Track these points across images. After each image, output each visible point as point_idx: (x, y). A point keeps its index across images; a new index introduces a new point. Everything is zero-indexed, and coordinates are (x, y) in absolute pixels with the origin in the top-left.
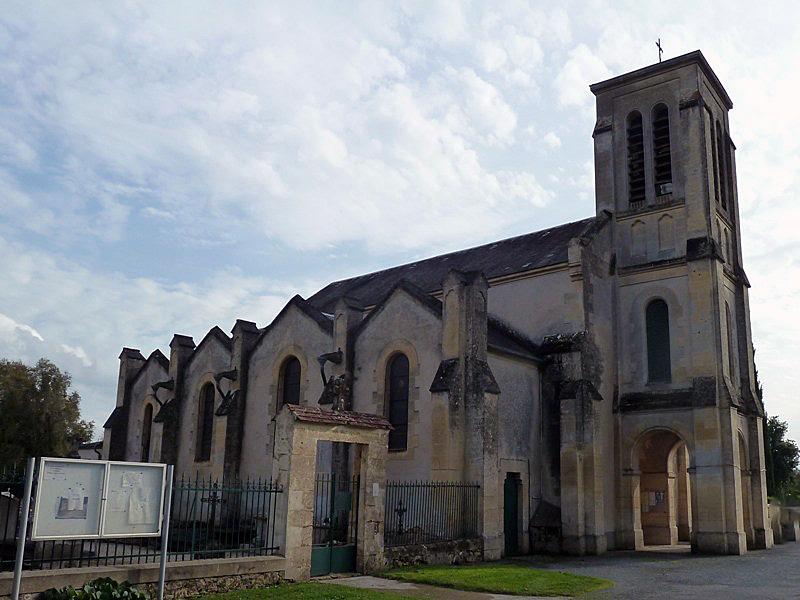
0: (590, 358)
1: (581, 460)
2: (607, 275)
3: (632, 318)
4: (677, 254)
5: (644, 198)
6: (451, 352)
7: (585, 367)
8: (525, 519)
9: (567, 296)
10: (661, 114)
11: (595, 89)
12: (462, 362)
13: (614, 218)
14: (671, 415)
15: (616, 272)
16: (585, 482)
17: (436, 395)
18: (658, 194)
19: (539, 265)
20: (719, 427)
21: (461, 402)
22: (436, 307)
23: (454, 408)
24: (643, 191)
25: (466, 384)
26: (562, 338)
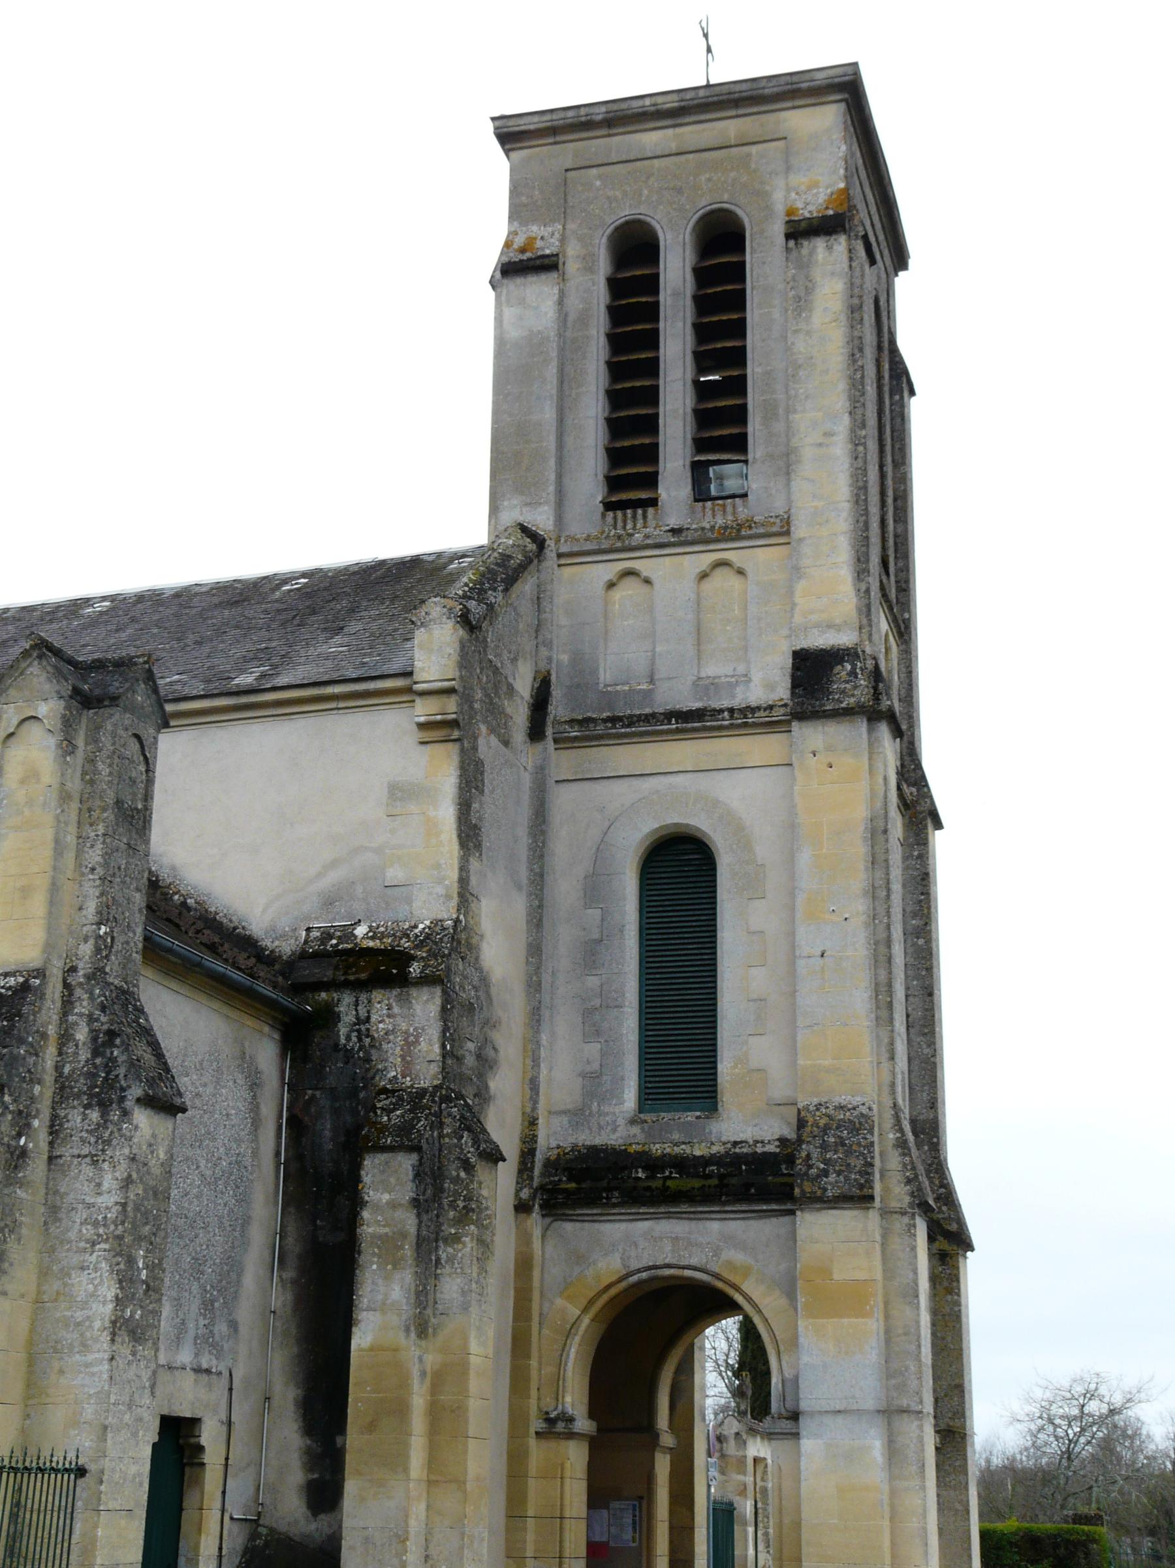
1: (423, 1374)
3: (595, 889)
4: (755, 694)
5: (654, 502)
7: (449, 1035)
9: (399, 793)
10: (721, 239)
11: (512, 134)
12: (54, 990)
13: (550, 553)
14: (715, 1226)
15: (549, 731)
16: (433, 1461)
18: (701, 494)
20: (879, 1276)
24: (651, 481)
25: (58, 1068)
26: (374, 934)
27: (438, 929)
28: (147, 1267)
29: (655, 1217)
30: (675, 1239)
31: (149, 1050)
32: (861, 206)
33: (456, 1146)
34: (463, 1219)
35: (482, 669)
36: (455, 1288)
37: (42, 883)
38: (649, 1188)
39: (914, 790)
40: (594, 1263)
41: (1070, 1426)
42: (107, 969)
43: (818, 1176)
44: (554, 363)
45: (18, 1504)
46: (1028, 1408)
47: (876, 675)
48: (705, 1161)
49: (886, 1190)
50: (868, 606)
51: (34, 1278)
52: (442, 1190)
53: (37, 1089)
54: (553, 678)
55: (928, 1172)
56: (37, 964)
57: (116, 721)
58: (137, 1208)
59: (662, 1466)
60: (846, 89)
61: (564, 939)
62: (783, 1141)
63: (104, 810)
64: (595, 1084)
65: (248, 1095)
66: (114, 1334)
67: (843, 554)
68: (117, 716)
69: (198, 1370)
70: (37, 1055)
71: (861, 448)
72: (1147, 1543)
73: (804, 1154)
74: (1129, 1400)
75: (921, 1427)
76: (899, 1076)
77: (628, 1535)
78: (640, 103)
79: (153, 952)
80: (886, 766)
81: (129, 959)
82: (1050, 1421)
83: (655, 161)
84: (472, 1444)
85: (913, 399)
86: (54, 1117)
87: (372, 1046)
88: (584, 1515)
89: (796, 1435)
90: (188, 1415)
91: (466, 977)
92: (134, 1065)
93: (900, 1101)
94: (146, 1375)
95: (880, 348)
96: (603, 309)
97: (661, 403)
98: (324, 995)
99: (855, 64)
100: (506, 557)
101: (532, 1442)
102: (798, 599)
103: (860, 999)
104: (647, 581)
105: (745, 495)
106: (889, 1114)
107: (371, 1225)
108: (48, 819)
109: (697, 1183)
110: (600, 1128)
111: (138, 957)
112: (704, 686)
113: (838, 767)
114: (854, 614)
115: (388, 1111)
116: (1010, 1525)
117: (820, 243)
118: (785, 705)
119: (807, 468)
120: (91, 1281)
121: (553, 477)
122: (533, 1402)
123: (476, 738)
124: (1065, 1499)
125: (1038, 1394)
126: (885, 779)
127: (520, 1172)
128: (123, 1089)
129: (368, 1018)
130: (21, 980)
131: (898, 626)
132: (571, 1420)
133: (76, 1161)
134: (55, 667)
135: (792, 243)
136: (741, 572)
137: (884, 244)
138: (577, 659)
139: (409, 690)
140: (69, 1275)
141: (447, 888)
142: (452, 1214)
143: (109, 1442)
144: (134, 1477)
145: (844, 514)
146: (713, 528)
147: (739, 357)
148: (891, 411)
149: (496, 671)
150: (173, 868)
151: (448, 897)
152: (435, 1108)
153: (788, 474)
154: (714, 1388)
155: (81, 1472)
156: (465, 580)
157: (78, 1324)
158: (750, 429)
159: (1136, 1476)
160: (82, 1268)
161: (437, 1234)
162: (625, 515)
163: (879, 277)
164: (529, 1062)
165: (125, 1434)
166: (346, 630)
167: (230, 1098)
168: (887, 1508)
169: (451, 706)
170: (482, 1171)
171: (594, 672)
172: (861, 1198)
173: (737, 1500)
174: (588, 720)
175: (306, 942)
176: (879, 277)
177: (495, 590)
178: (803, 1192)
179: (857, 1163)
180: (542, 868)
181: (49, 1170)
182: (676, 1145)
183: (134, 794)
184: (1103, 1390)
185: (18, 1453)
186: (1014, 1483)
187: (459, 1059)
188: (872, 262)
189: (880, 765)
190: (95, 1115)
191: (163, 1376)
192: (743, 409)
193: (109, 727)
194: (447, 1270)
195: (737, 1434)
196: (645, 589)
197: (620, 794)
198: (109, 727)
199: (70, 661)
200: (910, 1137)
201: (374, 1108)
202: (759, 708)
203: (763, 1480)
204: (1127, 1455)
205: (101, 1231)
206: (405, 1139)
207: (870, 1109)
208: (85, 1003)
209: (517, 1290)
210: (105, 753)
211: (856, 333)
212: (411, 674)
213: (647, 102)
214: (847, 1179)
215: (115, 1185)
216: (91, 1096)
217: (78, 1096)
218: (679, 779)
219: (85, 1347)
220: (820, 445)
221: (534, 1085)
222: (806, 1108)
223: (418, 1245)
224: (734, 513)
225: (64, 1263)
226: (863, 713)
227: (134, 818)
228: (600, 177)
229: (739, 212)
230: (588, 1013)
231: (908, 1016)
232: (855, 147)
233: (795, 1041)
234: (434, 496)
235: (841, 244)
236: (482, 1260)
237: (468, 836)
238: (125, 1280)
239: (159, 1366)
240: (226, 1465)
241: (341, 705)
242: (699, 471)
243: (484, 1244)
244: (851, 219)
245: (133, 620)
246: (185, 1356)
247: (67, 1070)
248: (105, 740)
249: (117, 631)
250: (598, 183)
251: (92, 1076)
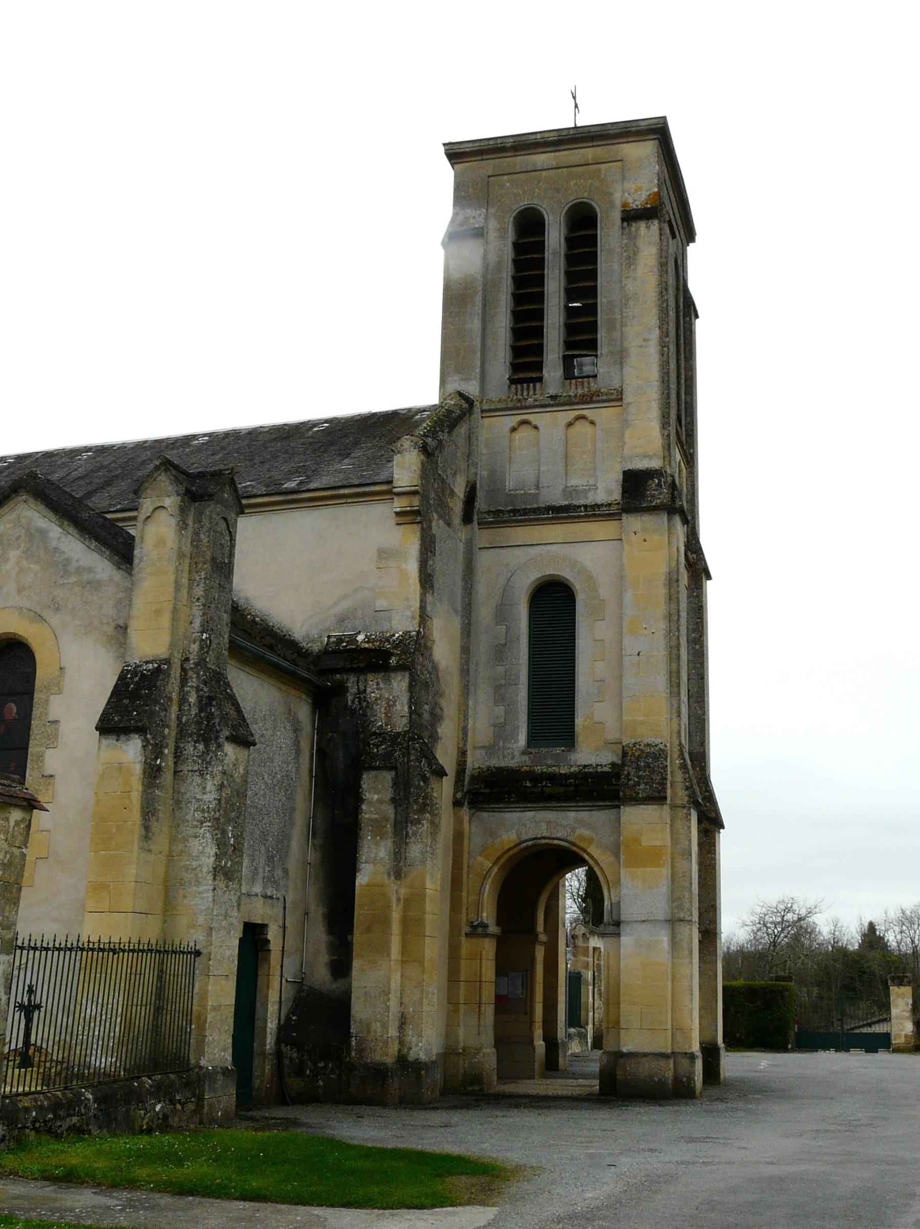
0: (423, 687)
1: (399, 900)
2: (457, 520)
3: (502, 613)
4: (600, 497)
5: (540, 379)
6: (150, 643)
7: (414, 701)
8: (272, 1025)
9: (384, 554)
10: (583, 221)
11: (456, 154)
12: (176, 672)
14: (572, 815)
17: (110, 741)
18: (569, 374)
19: (313, 486)
20: (669, 843)
21: (167, 762)
22: (122, 551)
23: (152, 773)
24: (539, 366)
25: (179, 718)
26: (368, 640)
27: (407, 637)
28: (233, 836)
29: (536, 809)
31: (233, 708)
32: (667, 202)
33: (418, 767)
34: (423, 809)
35: (435, 479)
36: (418, 850)
37: (168, 607)
38: (533, 793)
39: (695, 556)
40: (501, 836)
41: (775, 927)
42: (208, 660)
43: (634, 785)
44: (480, 294)
45: (162, 971)
46: (752, 918)
47: (673, 486)
48: (567, 776)
49: (674, 794)
50: (669, 445)
51: (167, 842)
52: (410, 793)
53: (166, 731)
54: (478, 485)
55: (698, 783)
56: (165, 656)
57: (212, 510)
58: (227, 803)
59: (540, 953)
60: (658, 132)
61: (483, 645)
62: (613, 765)
63: (205, 563)
64: (501, 730)
65: (292, 735)
66: (215, 875)
67: (654, 414)
68: (212, 507)
69: (265, 897)
70: (166, 710)
71: (666, 349)
72: (816, 990)
73: (626, 772)
74: (809, 913)
75: (691, 930)
76: (683, 727)
77: (519, 991)
78: (534, 137)
79: (235, 650)
80: (678, 541)
81: (221, 653)
82: (765, 925)
83: (544, 173)
84: (427, 940)
85: (697, 320)
86: (177, 748)
87: (367, 707)
88: (493, 980)
89: (619, 935)
90: (260, 922)
91: (424, 666)
92: (224, 717)
93: (683, 742)
94: (234, 899)
95: (678, 289)
96: (510, 260)
97: (545, 302)
98: (338, 676)
99: (665, 117)
100: (450, 412)
101: (463, 939)
102: (626, 439)
103: (660, 681)
104: (536, 428)
105: (596, 376)
106: (676, 750)
107: (368, 813)
108: (171, 569)
109: (562, 790)
110: (504, 757)
111: (226, 653)
112: (569, 491)
113: (647, 542)
114: (661, 450)
115: (377, 746)
116: (740, 982)
117: (642, 225)
118: (618, 504)
119: (633, 360)
120: (201, 844)
121: (479, 363)
122: (464, 916)
123: (430, 521)
124: (772, 968)
125: (759, 910)
126: (678, 549)
127: (456, 782)
128: (218, 732)
129: (365, 690)
130: (156, 665)
131: (686, 457)
132: (486, 926)
133: (190, 774)
134: (174, 476)
135: (625, 224)
136: (592, 423)
137: (681, 227)
138: (492, 474)
139: (390, 492)
140: (188, 840)
141: (413, 612)
142: (415, 807)
143: (214, 937)
144: (229, 958)
145: (655, 389)
146: (576, 396)
147: (592, 292)
148: (684, 328)
149: (443, 481)
150: (247, 599)
151: (413, 618)
152: (405, 745)
153: (622, 363)
154: (570, 909)
155: (198, 953)
156: (425, 425)
157: (194, 869)
158: (599, 336)
159: (812, 954)
160: (196, 837)
161: (407, 818)
162: (523, 387)
163: (678, 246)
164: (462, 717)
165: (223, 932)
166: (352, 455)
167: (282, 738)
168: (670, 975)
169: (416, 501)
170: (434, 782)
171: (503, 481)
172: (658, 798)
173: (583, 971)
174: (499, 511)
175: (327, 644)
176: (678, 246)
177: (443, 432)
178: (625, 795)
179: (657, 778)
180: (470, 600)
181: (175, 779)
182: (551, 767)
183: (223, 554)
184: (795, 907)
185: (161, 942)
186: (745, 960)
187: (420, 715)
188: (674, 237)
189: (675, 541)
190: (201, 747)
191: (245, 900)
192: (595, 323)
193: (208, 513)
194: (413, 839)
195: (584, 934)
196: (534, 432)
197: (518, 556)
198: (208, 513)
199: (184, 473)
200: (689, 762)
201: (369, 744)
202: (602, 505)
203: (598, 960)
204: (807, 942)
205: (206, 815)
207: (666, 746)
208: (194, 680)
209: (454, 852)
210: (205, 529)
211: (664, 280)
212: (391, 482)
213: (539, 136)
214: (651, 787)
215: (214, 788)
216: (199, 735)
217: (191, 735)
218: (554, 547)
219: (198, 883)
220: (641, 346)
221: (464, 731)
222: (628, 745)
223: (395, 825)
224: (589, 387)
225: (185, 834)
226: (665, 509)
227: (223, 568)
228: (509, 181)
229: (594, 204)
230: (497, 689)
231: (689, 691)
232: (664, 167)
233: (621, 706)
234: (406, 373)
235: (655, 225)
236: (434, 834)
237: (425, 581)
238: (221, 844)
239: (242, 894)
240: (283, 951)
241: (349, 501)
242: (568, 361)
243: (435, 825)
244: (661, 210)
245: (223, 448)
246: (257, 889)
247: (184, 720)
248: (205, 521)
249: (213, 455)
250: (508, 185)
251: (199, 723)
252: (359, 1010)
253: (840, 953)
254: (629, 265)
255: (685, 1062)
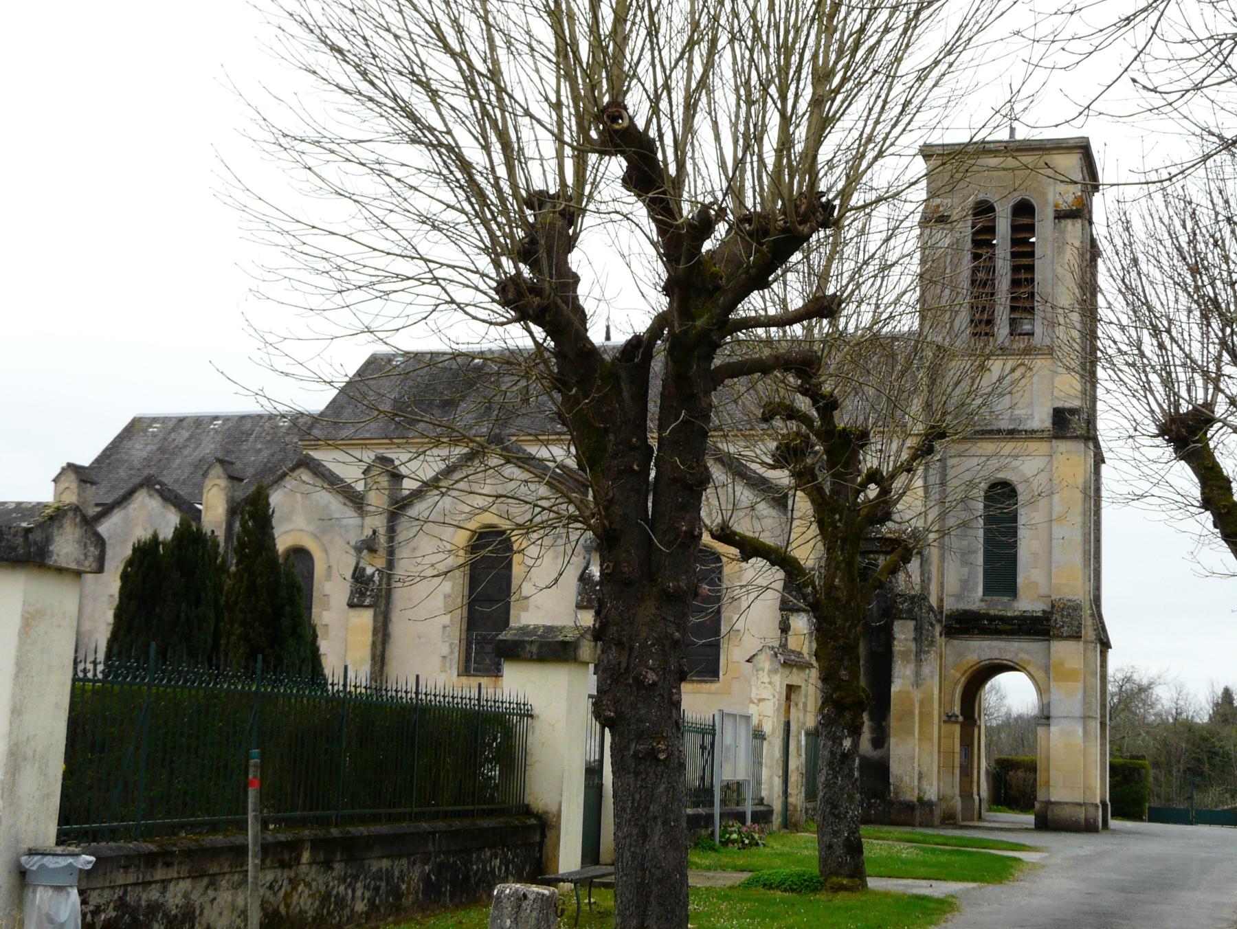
10: (1024, 210)
14: (1016, 644)
30: (1000, 649)
62: (1044, 611)
64: (966, 584)
107: (898, 647)
109: (1009, 627)
117: (1069, 222)
172: (1076, 636)
206: (910, 615)
242: (1013, 322)
252: (895, 768)
253: (1184, 727)
254: (1059, 253)
255: (1092, 809)
